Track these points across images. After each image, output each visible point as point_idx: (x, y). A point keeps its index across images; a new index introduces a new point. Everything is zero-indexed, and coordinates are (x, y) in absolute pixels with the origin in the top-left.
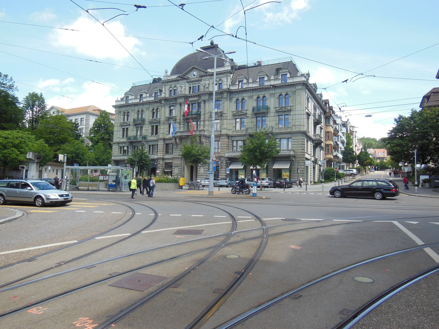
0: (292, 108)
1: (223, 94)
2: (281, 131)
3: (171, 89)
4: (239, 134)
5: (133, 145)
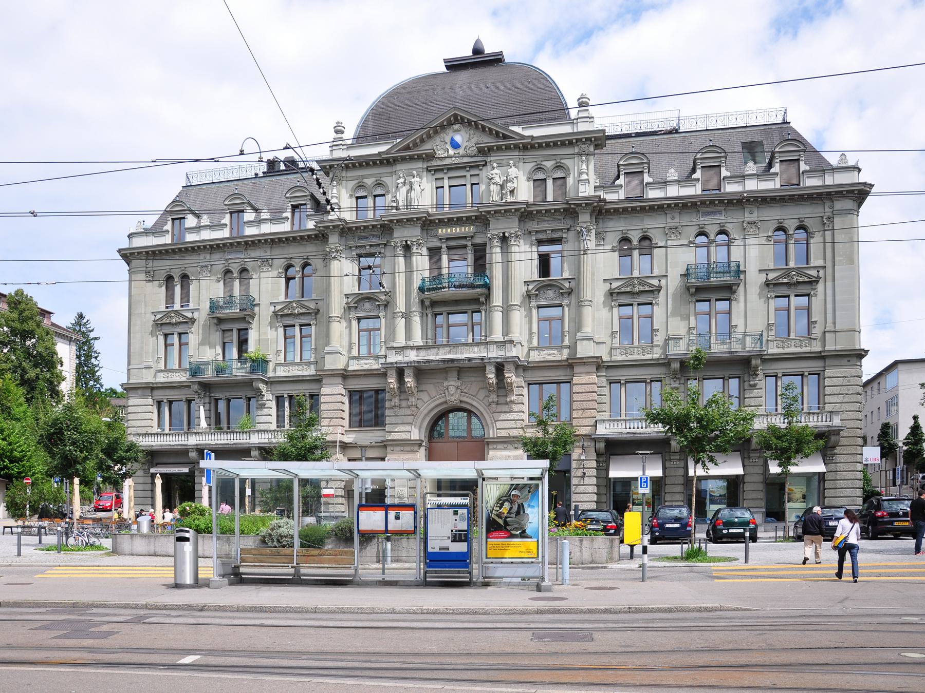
0: (821, 273)
1: (392, 233)
2: (787, 350)
3: (540, 176)
4: (636, 357)
5: (210, 397)
